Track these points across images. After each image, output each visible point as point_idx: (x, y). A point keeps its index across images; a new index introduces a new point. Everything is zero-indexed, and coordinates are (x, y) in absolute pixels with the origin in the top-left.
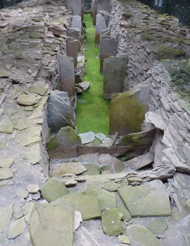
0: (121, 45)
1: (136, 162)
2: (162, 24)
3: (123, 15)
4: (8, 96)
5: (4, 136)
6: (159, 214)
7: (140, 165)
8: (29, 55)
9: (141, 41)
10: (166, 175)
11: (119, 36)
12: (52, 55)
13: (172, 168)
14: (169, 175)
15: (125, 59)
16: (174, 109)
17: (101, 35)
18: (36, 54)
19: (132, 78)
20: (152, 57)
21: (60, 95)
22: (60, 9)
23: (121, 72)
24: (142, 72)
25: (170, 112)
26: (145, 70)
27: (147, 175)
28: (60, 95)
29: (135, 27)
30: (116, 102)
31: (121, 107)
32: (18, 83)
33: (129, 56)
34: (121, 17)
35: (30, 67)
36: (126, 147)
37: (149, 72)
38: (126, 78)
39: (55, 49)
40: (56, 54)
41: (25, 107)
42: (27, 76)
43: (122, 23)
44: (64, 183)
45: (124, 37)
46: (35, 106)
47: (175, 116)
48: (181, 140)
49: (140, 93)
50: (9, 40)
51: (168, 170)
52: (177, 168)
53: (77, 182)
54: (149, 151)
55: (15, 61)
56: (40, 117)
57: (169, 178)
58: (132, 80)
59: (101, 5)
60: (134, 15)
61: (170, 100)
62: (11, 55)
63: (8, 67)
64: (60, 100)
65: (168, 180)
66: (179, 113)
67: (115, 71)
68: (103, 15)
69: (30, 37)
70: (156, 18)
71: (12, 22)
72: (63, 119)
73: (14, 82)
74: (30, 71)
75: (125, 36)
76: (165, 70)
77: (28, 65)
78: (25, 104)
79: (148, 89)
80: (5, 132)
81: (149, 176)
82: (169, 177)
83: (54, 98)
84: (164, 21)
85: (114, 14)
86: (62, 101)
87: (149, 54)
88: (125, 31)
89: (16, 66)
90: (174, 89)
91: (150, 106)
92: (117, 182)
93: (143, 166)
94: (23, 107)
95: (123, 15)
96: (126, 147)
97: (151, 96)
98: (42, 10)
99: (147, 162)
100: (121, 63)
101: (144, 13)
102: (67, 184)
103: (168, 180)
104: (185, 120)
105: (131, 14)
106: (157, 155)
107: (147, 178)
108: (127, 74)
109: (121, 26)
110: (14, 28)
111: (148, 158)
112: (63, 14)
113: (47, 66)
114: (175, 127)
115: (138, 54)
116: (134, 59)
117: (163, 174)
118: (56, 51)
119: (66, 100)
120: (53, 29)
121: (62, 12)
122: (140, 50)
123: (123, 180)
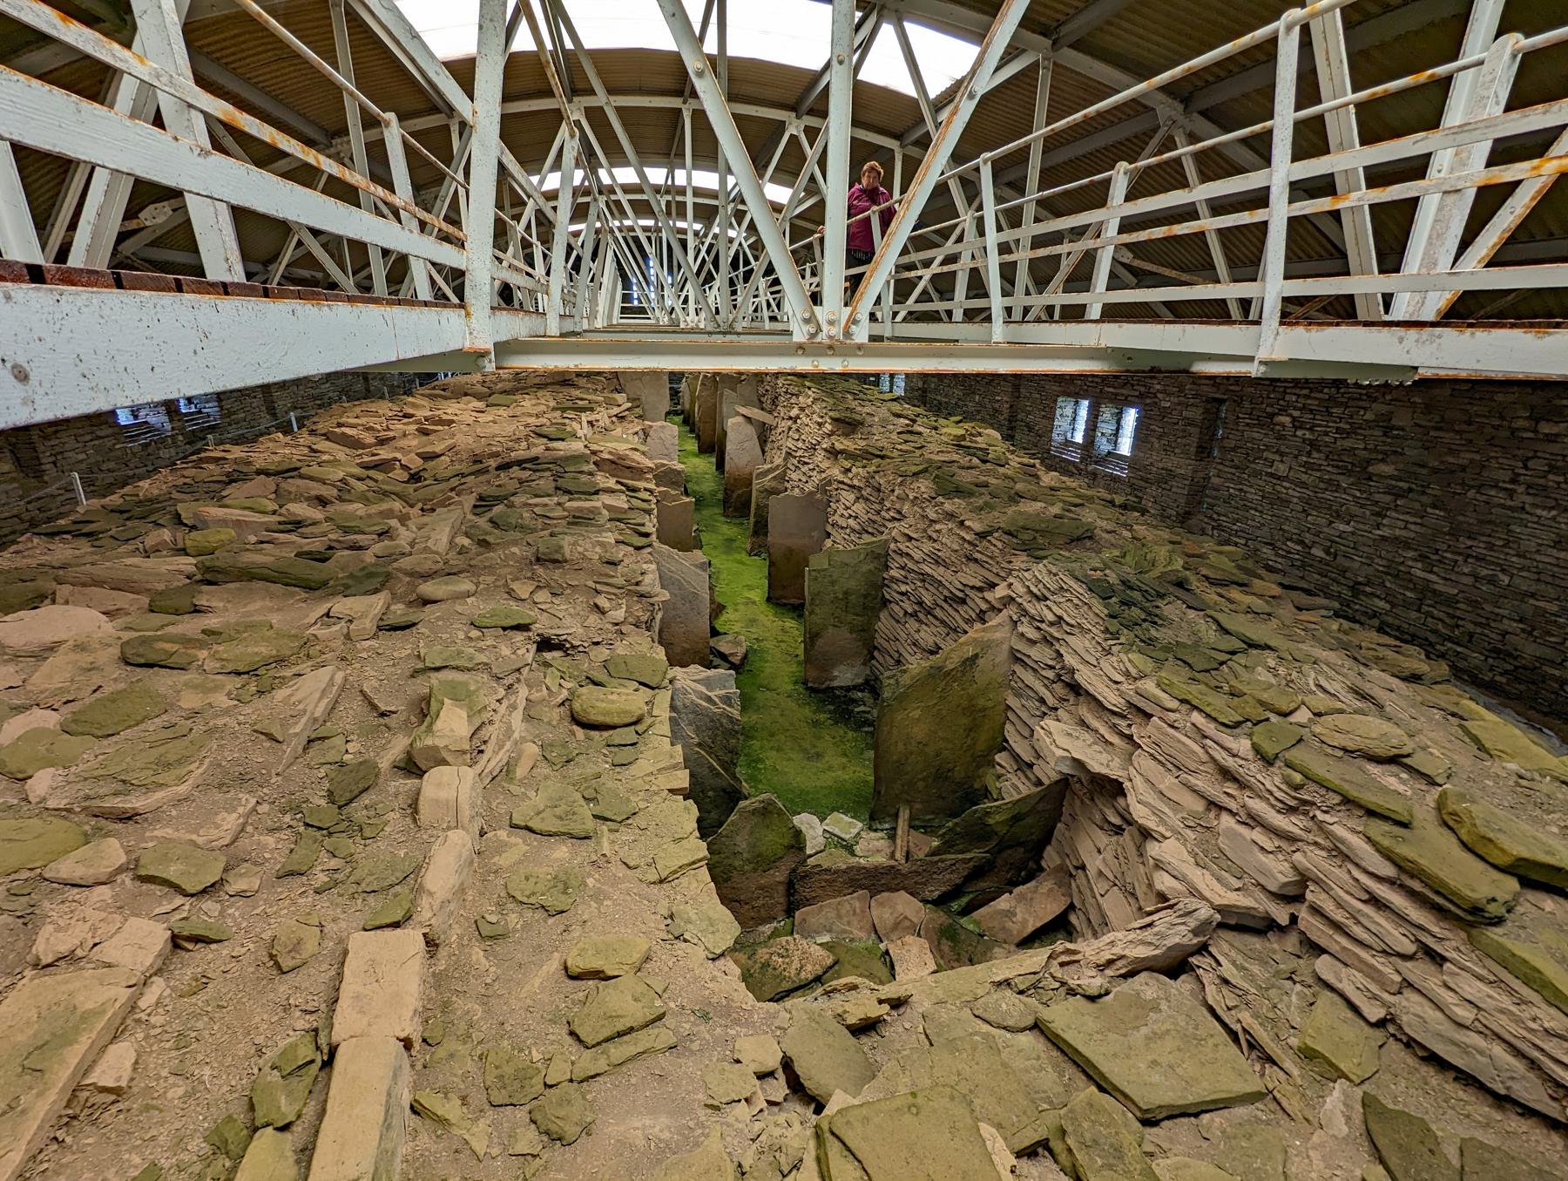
0: (841, 511)
1: (1010, 914)
2: (959, 444)
3: (834, 420)
4: (535, 696)
5: (564, 849)
6: (1224, 1095)
7: (1025, 921)
8: (580, 549)
9: (940, 499)
10: (1185, 941)
11: (829, 483)
12: (638, 548)
13: (1205, 912)
14: (1195, 941)
15: (878, 557)
16: (1142, 704)
17: (755, 482)
18: (602, 544)
19: (914, 615)
20: (999, 545)
21: (707, 682)
22: (610, 403)
23: (865, 596)
24: (960, 595)
25: (1124, 717)
26: (973, 588)
27: (1118, 950)
28: (707, 682)
29: (883, 457)
30: (902, 698)
31: (917, 714)
32: (559, 647)
33: (892, 546)
34: (828, 427)
35: (599, 587)
36: (968, 856)
37: (1001, 591)
38: (883, 615)
39: (642, 529)
40: (650, 545)
41: (606, 734)
42: (594, 619)
43: (838, 446)
44: (840, 1017)
45: (853, 487)
46: (640, 728)
47: (1159, 728)
48: (1199, 806)
49: (980, 661)
50: (481, 498)
51: (1192, 923)
52: (1220, 909)
53: (886, 1007)
54: (1042, 870)
55: (540, 570)
56: (675, 767)
57: (1192, 955)
58: (911, 621)
59: (734, 390)
60: (869, 419)
61: (1119, 678)
62: (515, 549)
63: (523, 589)
64: (709, 699)
65: (1194, 960)
66: (1172, 716)
67: (846, 593)
68: (748, 419)
69: (557, 488)
70: (936, 429)
71: (464, 440)
72: (712, 768)
73: (545, 644)
74: (602, 601)
75: (856, 482)
76: (1072, 583)
77: (591, 584)
78: (608, 720)
79: (1005, 647)
80: (564, 834)
81: (1127, 952)
82: (1388, 913)
83: (685, 693)
84: (963, 437)
85: (798, 417)
86: (715, 704)
87: (982, 536)
88: (854, 470)
89: (548, 586)
90: (1123, 640)
91: (1012, 701)
92: (1021, 992)
93: (1039, 924)
94: (595, 734)
95: (834, 420)
96: (968, 856)
97: (1018, 668)
98: (552, 404)
99: (1049, 909)
100: (865, 568)
101: (899, 416)
102: (852, 1020)
103: (1194, 960)
104: (1198, 738)
105: (858, 417)
106: (1101, 873)
107: (1119, 964)
108: (885, 603)
109: (833, 453)
110: (475, 462)
111: (1051, 890)
112: (621, 418)
113: (637, 584)
114: (1163, 765)
115: (930, 538)
116: (917, 555)
117: (1177, 940)
118: (647, 535)
119: (727, 700)
120: (613, 462)
121: (616, 410)
122: (938, 527)
123: (1039, 981)
